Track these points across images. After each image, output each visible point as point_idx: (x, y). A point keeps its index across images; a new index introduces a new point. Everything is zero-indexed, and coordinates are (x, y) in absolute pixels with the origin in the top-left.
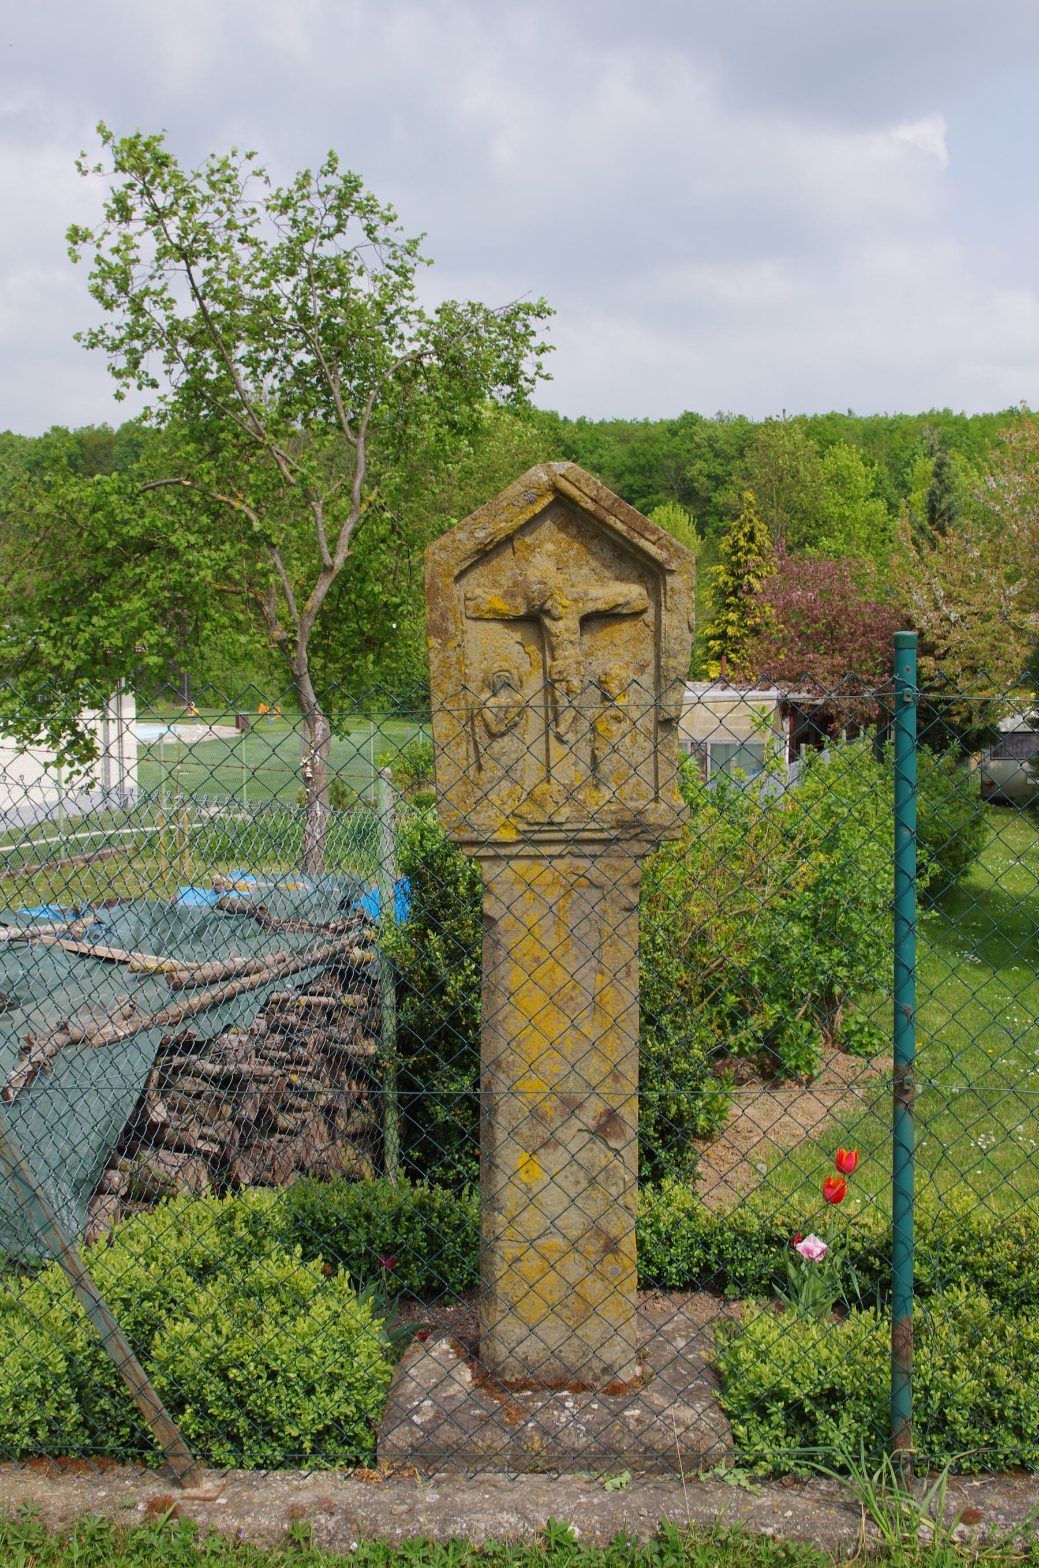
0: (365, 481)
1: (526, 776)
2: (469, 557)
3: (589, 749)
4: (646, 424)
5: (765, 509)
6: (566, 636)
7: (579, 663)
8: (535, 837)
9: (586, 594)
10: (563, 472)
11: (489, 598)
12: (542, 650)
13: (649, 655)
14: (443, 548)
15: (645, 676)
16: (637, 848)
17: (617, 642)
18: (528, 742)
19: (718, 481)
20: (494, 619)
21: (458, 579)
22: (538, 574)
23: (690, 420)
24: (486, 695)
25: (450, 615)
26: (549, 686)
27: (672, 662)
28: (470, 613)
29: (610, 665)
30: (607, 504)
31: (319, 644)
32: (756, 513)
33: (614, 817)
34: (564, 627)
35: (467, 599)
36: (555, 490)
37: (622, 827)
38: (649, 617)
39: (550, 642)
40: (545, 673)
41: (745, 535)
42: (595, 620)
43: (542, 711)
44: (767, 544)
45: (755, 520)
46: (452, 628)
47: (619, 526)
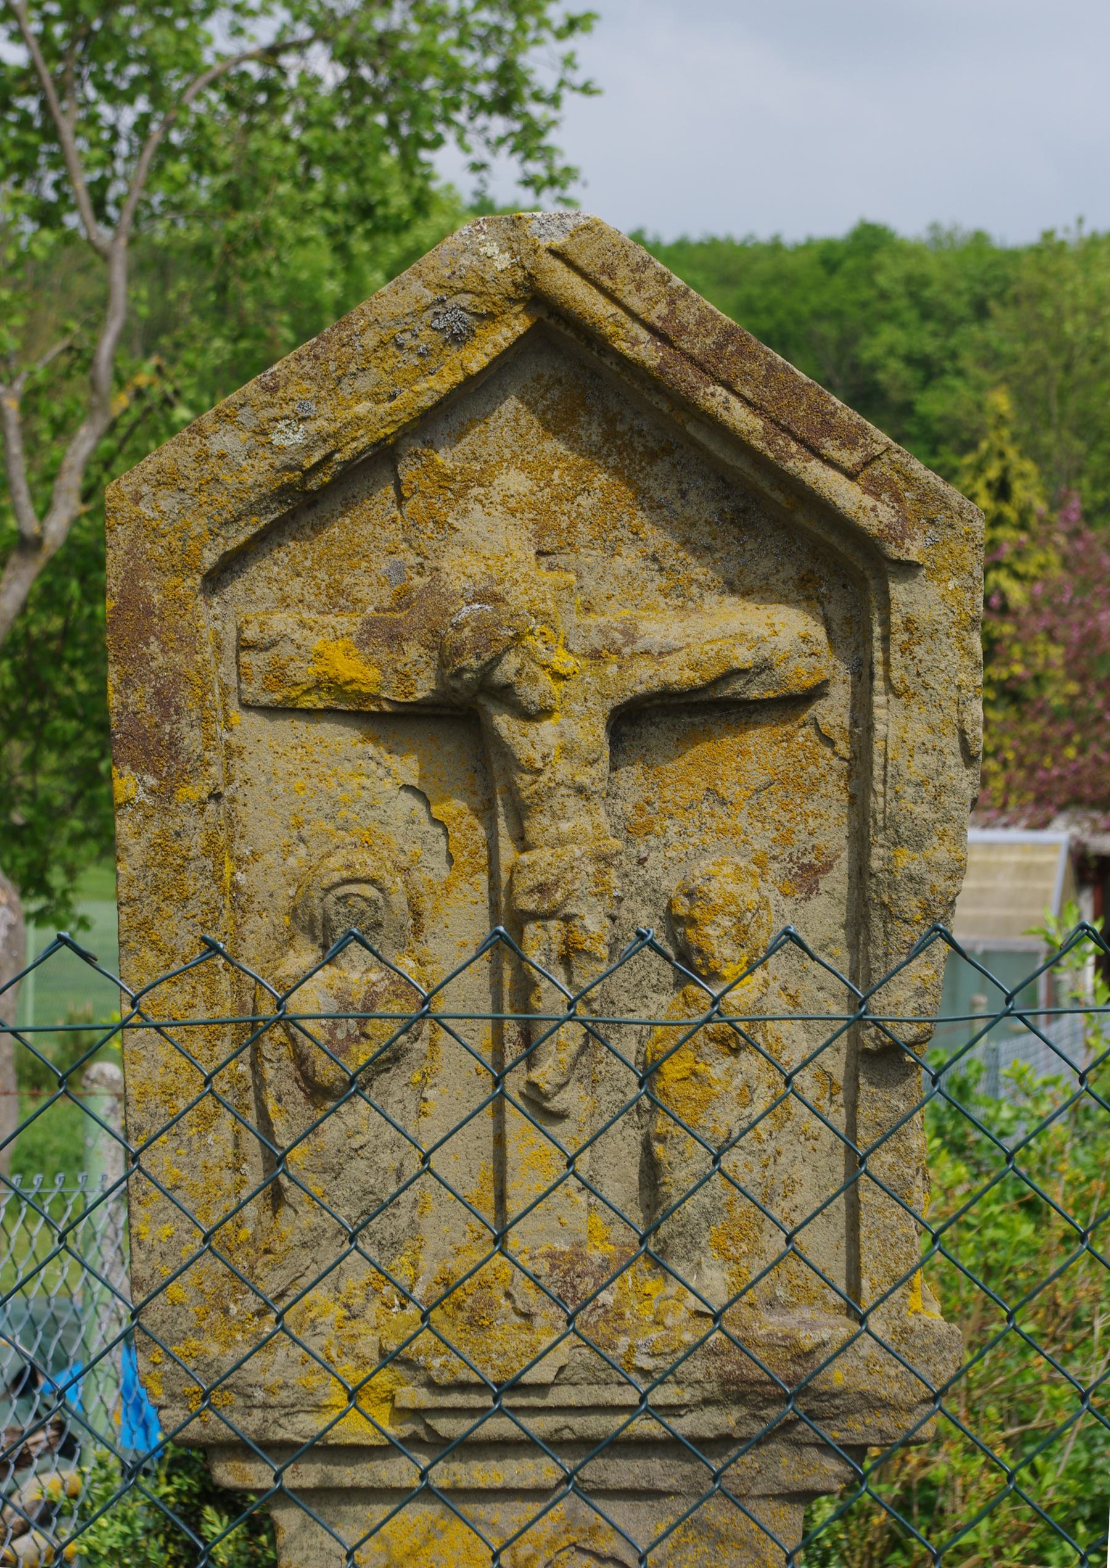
0: (124, 339)
1: (427, 1224)
2: (251, 510)
3: (634, 1136)
4: (775, 247)
5: (1034, 431)
6: (564, 770)
7: (604, 859)
8: (456, 1429)
9: (630, 636)
10: (559, 241)
11: (317, 643)
12: (486, 812)
13: (834, 837)
14: (168, 480)
15: (818, 903)
16: (787, 1467)
17: (730, 790)
18: (429, 1132)
19: (928, 370)
20: (330, 713)
21: (216, 579)
22: (476, 568)
23: (870, 239)
24: (301, 957)
25: (186, 699)
26: (504, 941)
27: (907, 860)
28: (252, 691)
29: (705, 865)
30: (699, 346)
31: (23, 712)
32: (1015, 438)
33: (714, 1365)
34: (558, 741)
35: (244, 646)
36: (534, 297)
37: (740, 1399)
38: (833, 711)
39: (512, 791)
40: (493, 887)
41: (989, 485)
42: (655, 720)
43: (481, 1036)
44: (1040, 506)
45: (1012, 453)
46: (192, 739)
47: (740, 417)
